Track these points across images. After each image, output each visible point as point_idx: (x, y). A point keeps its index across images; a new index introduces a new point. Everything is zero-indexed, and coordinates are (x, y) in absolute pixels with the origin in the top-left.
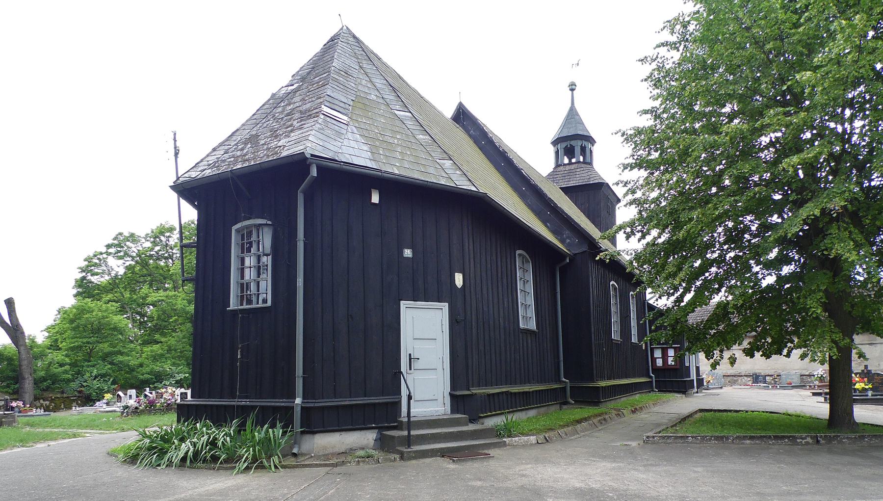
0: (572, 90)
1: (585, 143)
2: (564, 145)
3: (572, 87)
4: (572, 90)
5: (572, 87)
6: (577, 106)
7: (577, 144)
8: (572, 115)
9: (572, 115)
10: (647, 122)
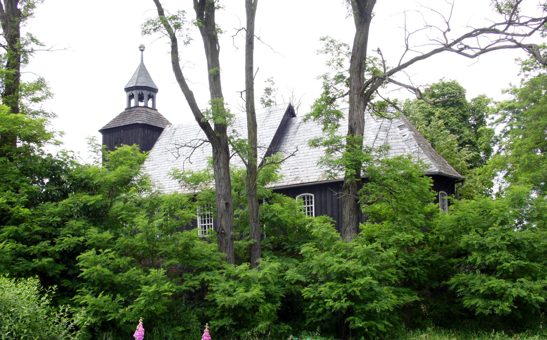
0: (142, 51)
1: (153, 93)
2: (138, 92)
3: (142, 49)
4: (142, 51)
5: (142, 49)
6: (144, 62)
7: (146, 93)
8: (142, 70)
9: (142, 70)
10: (509, 97)
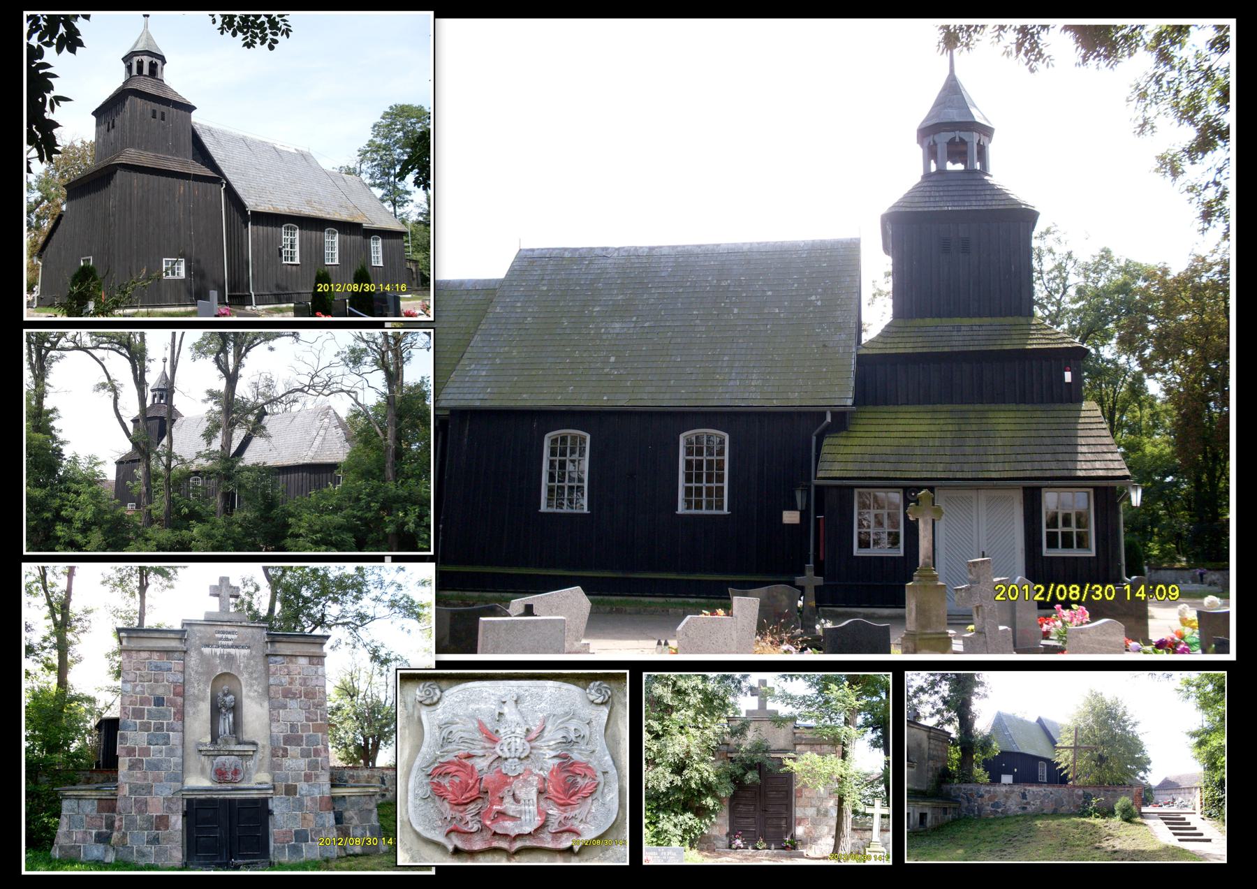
1: (159, 62)
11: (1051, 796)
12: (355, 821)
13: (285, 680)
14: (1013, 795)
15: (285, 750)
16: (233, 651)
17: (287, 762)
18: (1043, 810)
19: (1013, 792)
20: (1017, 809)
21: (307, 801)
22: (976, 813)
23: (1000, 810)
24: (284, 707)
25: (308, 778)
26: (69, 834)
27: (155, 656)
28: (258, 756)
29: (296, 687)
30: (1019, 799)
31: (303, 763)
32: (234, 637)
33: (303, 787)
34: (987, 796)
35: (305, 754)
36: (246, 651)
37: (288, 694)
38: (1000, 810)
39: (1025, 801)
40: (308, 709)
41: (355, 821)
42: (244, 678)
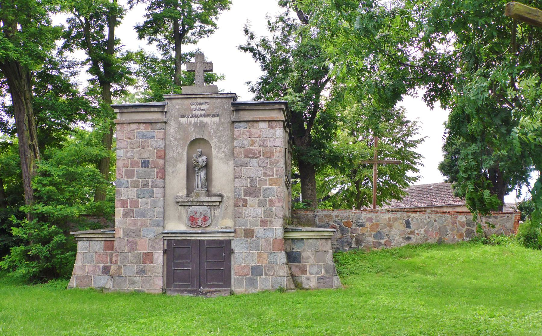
11: (436, 224)
12: (312, 260)
13: (247, 142)
14: (396, 224)
15: (246, 201)
16: (204, 119)
17: (246, 211)
18: (427, 240)
19: (396, 219)
20: (401, 240)
21: (262, 242)
22: (354, 245)
23: (383, 242)
24: (246, 165)
25: (263, 223)
26: (83, 267)
27: (142, 127)
28: (223, 206)
29: (256, 148)
30: (402, 228)
31: (259, 211)
32: (206, 107)
33: (259, 231)
34: (368, 225)
35: (262, 204)
36: (216, 119)
37: (249, 154)
38: (383, 242)
39: (409, 230)
40: (265, 167)
41: (312, 260)
42: (213, 142)
